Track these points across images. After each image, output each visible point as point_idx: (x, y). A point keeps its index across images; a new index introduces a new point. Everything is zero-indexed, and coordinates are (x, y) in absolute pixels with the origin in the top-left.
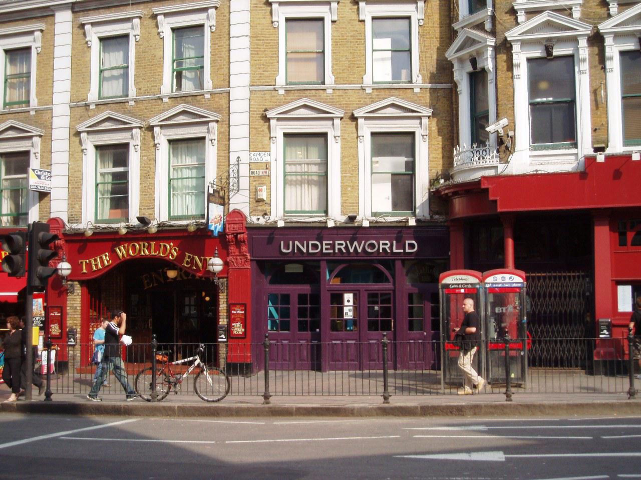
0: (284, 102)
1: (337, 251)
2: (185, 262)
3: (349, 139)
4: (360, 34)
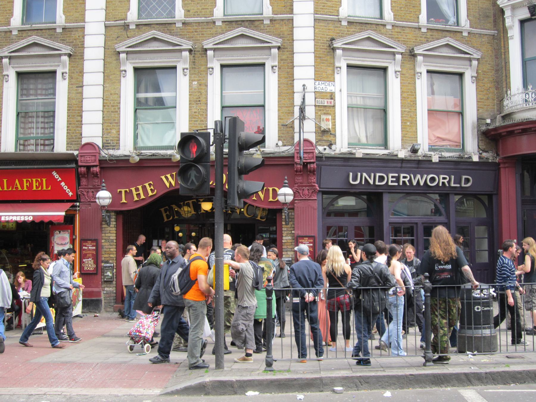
0: (346, 34)
1: (401, 184)
3: (407, 75)
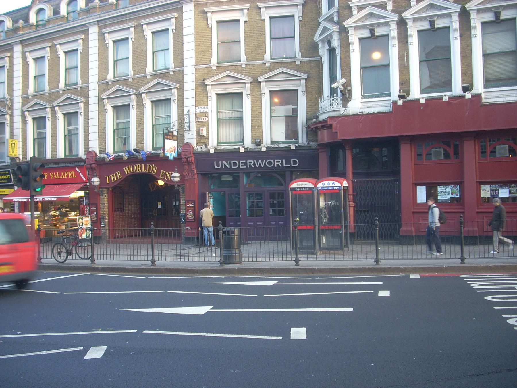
0: (215, 74)
1: (248, 167)
2: (161, 175)
3: (256, 95)
4: (262, 28)
